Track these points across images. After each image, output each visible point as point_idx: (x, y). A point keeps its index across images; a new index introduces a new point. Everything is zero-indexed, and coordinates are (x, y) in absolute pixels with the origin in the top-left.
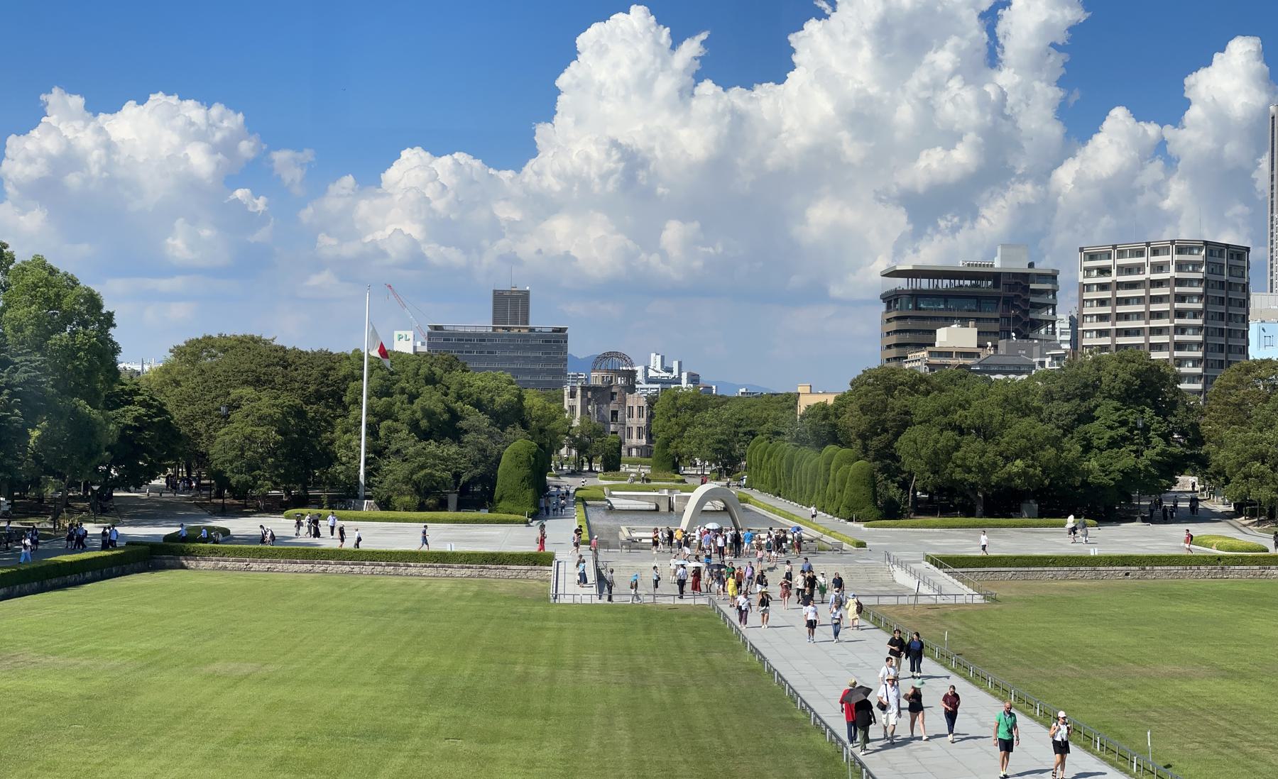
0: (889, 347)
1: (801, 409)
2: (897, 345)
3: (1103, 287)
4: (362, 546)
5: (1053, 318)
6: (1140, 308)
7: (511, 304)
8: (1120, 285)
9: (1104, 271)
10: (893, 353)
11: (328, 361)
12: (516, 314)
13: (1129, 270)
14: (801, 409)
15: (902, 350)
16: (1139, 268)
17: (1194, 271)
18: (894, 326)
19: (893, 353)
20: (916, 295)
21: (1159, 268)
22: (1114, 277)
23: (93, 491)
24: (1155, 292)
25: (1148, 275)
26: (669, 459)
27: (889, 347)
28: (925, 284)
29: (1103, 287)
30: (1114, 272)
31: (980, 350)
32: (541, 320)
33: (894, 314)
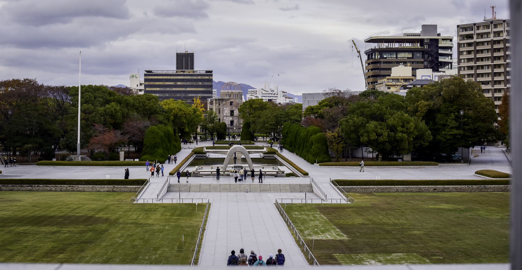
0: (369, 77)
1: (304, 110)
2: (373, 76)
3: (470, 45)
4: (131, 177)
5: (451, 61)
6: (489, 63)
7: (185, 60)
8: (478, 44)
9: (470, 37)
10: (371, 80)
11: (74, 88)
12: (188, 65)
13: (481, 35)
14: (304, 110)
15: (374, 78)
16: (488, 34)
17: (487, 37)
18: (371, 66)
19: (371, 80)
20: (381, 51)
21: (498, 34)
22: (475, 39)
23: (497, 121)
24: (496, 46)
25: (492, 37)
26: (248, 136)
27: (369, 77)
28: (385, 45)
29: (470, 45)
30: (475, 37)
31: (413, 77)
32: (200, 67)
33: (371, 61)
